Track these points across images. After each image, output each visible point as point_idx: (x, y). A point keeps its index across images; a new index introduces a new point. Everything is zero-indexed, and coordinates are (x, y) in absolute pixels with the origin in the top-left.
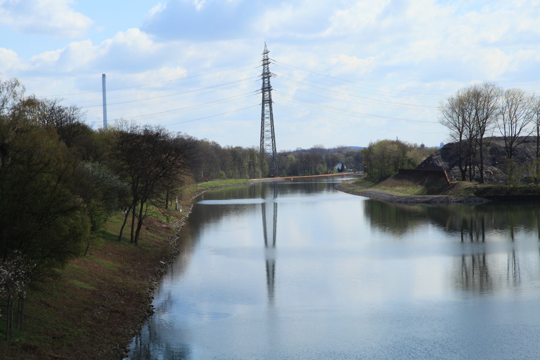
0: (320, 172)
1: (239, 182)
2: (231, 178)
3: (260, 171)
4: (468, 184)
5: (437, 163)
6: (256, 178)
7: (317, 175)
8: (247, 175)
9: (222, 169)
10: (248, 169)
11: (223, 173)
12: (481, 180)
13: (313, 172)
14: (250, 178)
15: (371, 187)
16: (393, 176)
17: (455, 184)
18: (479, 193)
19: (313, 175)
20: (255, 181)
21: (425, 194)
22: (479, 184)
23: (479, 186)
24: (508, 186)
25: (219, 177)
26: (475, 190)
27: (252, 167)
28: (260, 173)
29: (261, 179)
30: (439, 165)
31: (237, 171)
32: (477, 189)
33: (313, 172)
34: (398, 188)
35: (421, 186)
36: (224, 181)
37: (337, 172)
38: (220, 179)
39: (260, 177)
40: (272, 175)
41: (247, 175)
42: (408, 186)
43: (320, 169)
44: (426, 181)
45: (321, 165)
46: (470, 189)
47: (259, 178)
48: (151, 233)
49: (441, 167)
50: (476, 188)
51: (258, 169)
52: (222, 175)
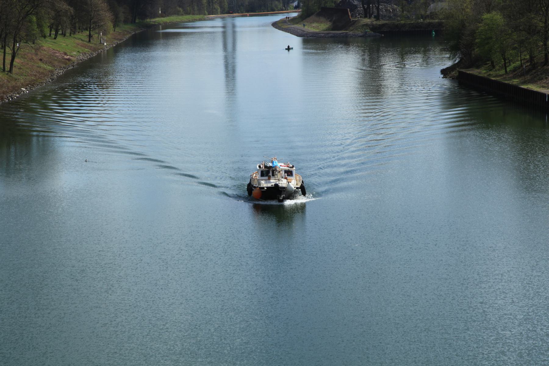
0: (276, 9)
1: (195, 18)
2: (189, 14)
3: (219, 8)
4: (367, 21)
5: (352, 1)
6: (214, 14)
7: (273, 11)
8: (205, 11)
9: (180, 7)
10: (206, 6)
11: (181, 9)
12: (377, 18)
13: (269, 9)
14: (209, 14)
15: (293, 24)
16: (316, 13)
17: (356, 21)
18: (374, 28)
19: (269, 12)
20: (212, 17)
21: (330, 30)
22: (375, 21)
23: (375, 23)
24: (399, 22)
25: (177, 13)
26: (371, 26)
27: (211, 4)
28: (219, 10)
29: (220, 15)
30: (354, 3)
31: (196, 7)
32: (373, 25)
33: (269, 9)
34: (314, 25)
35: (330, 23)
36: (180, 17)
37: (293, 9)
38: (177, 15)
39: (219, 13)
40: (231, 12)
41: (205, 11)
42: (321, 22)
43: (276, 6)
44: (334, 18)
45: (277, 2)
46: (367, 25)
47: (218, 14)
48: (42, 64)
49: (355, 5)
50: (372, 25)
51: (217, 6)
52: (180, 11)
